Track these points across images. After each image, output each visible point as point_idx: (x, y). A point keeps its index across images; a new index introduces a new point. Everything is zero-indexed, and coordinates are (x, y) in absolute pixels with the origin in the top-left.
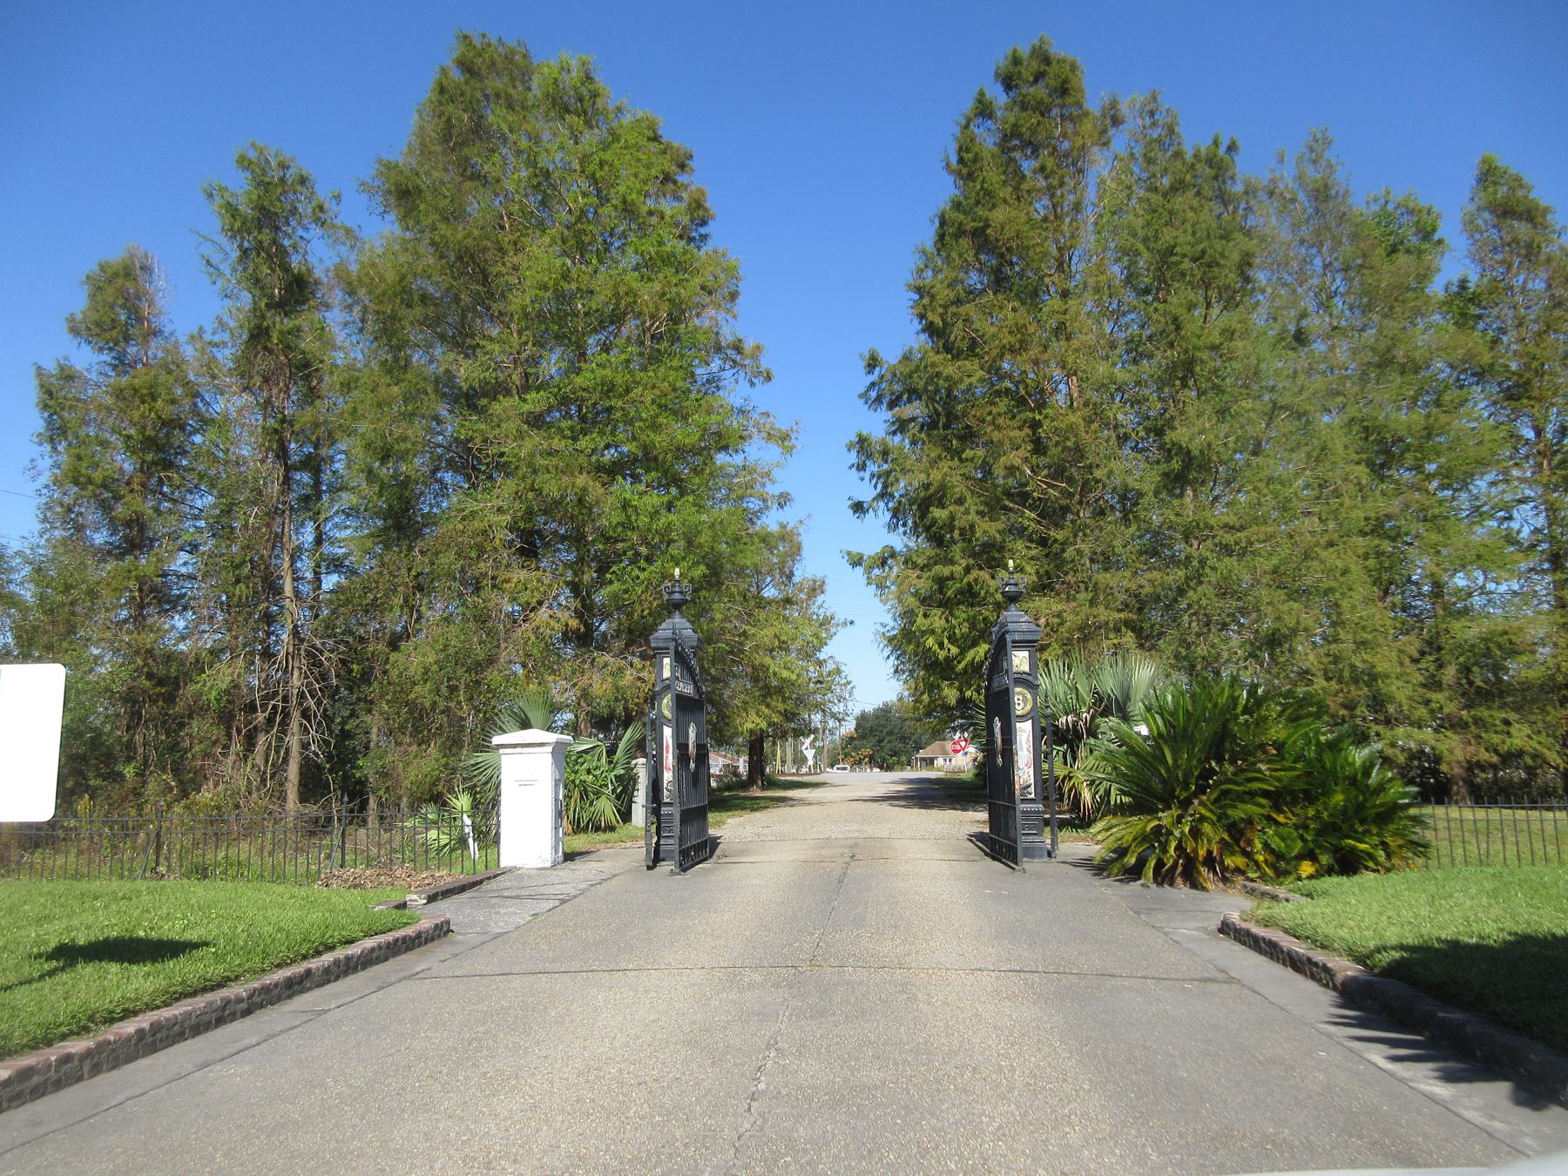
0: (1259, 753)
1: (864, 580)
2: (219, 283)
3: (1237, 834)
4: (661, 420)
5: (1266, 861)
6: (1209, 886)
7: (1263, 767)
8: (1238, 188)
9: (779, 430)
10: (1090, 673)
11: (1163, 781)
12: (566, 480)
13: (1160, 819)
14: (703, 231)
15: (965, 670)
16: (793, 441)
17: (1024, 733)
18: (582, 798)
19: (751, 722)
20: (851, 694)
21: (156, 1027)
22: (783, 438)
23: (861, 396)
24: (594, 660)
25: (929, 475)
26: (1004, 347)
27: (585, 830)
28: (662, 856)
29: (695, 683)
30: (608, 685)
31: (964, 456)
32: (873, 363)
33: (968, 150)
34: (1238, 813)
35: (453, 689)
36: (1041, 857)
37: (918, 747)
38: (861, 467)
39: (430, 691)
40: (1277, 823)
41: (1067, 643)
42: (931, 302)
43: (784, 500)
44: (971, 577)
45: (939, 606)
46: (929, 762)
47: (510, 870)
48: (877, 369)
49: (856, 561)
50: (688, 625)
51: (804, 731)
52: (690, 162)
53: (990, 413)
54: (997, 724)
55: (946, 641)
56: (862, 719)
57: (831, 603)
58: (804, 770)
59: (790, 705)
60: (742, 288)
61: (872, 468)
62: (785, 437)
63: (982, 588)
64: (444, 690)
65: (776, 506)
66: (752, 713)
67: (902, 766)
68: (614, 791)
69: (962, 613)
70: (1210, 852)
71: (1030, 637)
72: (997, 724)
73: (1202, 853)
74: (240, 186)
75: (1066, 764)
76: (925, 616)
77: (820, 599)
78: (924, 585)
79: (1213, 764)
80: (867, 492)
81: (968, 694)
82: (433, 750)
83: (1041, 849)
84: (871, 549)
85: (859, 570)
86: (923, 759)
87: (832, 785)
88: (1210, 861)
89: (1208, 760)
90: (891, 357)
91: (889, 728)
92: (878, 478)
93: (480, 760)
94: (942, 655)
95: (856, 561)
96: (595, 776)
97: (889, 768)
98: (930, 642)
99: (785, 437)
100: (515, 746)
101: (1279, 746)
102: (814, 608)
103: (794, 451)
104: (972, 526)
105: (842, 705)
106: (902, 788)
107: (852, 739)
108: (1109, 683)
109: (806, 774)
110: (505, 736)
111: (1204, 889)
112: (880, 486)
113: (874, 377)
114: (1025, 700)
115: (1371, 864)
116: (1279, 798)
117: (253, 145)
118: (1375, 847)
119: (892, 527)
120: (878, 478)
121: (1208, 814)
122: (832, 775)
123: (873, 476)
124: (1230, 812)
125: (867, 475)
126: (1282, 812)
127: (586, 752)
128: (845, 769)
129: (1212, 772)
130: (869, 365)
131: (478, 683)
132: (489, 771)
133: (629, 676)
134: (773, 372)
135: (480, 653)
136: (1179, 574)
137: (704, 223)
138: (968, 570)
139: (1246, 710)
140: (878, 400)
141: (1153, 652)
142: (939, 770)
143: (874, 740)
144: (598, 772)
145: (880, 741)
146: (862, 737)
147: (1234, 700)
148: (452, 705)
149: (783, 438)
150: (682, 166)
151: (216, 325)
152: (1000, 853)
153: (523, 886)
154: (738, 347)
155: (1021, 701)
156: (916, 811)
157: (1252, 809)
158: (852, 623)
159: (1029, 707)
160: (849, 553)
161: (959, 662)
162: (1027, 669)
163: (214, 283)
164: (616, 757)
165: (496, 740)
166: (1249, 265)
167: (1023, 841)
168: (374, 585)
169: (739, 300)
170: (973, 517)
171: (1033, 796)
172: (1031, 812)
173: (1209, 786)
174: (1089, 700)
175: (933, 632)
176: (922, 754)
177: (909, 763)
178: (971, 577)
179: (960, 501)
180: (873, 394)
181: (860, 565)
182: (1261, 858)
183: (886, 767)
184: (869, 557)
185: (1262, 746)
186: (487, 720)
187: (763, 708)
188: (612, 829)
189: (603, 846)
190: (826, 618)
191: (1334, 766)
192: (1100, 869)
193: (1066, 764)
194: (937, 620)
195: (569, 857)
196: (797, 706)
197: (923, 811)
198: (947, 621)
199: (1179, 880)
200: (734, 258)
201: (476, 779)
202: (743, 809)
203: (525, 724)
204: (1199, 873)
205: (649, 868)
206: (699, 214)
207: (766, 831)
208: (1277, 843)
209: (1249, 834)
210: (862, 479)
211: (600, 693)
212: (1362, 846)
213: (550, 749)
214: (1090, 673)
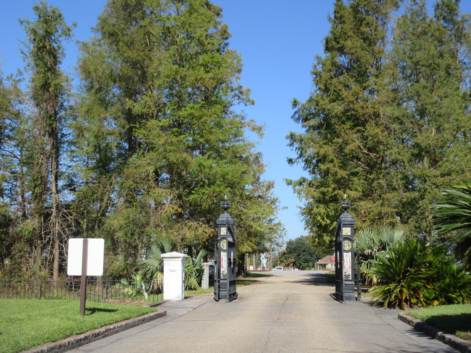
0: (423, 266)
1: (292, 191)
2: (27, 61)
3: (416, 291)
4: (214, 130)
5: (424, 301)
6: (405, 308)
7: (423, 270)
8: (459, 19)
9: (258, 126)
10: (379, 233)
11: (392, 274)
12: (178, 155)
13: (390, 286)
14: (226, 41)
15: (333, 230)
16: (263, 130)
17: (347, 258)
20: (285, 234)
21: (127, 324)
22: (258, 130)
23: (292, 117)
24: (186, 224)
26: (350, 102)
28: (220, 297)
31: (333, 141)
32: (295, 103)
33: (338, 13)
34: (414, 285)
35: (132, 234)
36: (353, 300)
37: (318, 259)
40: (427, 288)
41: (373, 221)
42: (320, 79)
44: (336, 192)
45: (323, 203)
46: (324, 266)
48: (297, 106)
49: (289, 183)
50: (230, 216)
51: (264, 250)
52: (221, 13)
53: (343, 128)
54: (338, 254)
55: (325, 218)
56: (290, 243)
57: (274, 193)
58: (259, 269)
60: (243, 68)
62: (260, 129)
63: (340, 197)
64: (129, 235)
66: (246, 244)
67: (310, 267)
68: (195, 275)
69: (332, 206)
70: (406, 297)
71: (351, 223)
72: (338, 254)
73: (404, 298)
74: (33, 17)
75: (368, 268)
76: (317, 207)
77: (272, 190)
78: (317, 194)
79: (409, 268)
80: (294, 155)
83: (353, 297)
84: (296, 178)
85: (291, 186)
87: (275, 276)
88: (406, 301)
89: (407, 267)
90: (303, 100)
92: (299, 149)
94: (323, 223)
95: (289, 183)
97: (303, 269)
98: (319, 218)
99: (260, 129)
101: (430, 263)
102: (269, 195)
103: (264, 135)
104: (336, 173)
105: (281, 239)
106: (308, 278)
107: (284, 253)
108: (385, 238)
109: (260, 271)
111: (404, 309)
112: (299, 152)
113: (296, 109)
114: (349, 245)
115: (456, 302)
116: (429, 280)
117: (41, 2)
118: (458, 296)
119: (305, 169)
120: (299, 149)
121: (404, 285)
122: (275, 271)
123: (296, 148)
124: (412, 284)
125: (294, 148)
126: (430, 285)
128: (280, 269)
129: (409, 271)
130: (294, 105)
132: (149, 266)
133: (200, 230)
134: (255, 101)
136: (416, 194)
137: (227, 38)
138: (334, 189)
139: (421, 251)
140: (299, 119)
141: (406, 225)
142: (328, 270)
143: (296, 254)
144: (189, 268)
145: (299, 255)
146: (290, 253)
147: (416, 247)
149: (258, 130)
150: (218, 15)
151: (18, 72)
152: (338, 298)
153: (175, 305)
155: (346, 245)
156: (312, 286)
157: (418, 283)
158: (287, 208)
159: (350, 248)
160: (286, 180)
161: (330, 226)
162: (350, 234)
163: (24, 61)
166: (450, 68)
167: (345, 295)
168: (96, 191)
169: (242, 73)
170: (337, 169)
171: (351, 279)
172: (349, 284)
173: (407, 276)
174: (378, 243)
175: (320, 214)
176: (320, 262)
177: (313, 266)
178: (336, 192)
179: (332, 161)
180: (297, 116)
181: (291, 184)
182: (422, 300)
183: (301, 268)
184: (295, 181)
185: (424, 263)
188: (195, 289)
189: (194, 295)
190: (274, 199)
191: (447, 270)
192: (371, 304)
193: (368, 268)
194: (322, 209)
195: (186, 298)
196: (261, 240)
197: (315, 286)
198: (326, 209)
199: (397, 307)
200: (239, 53)
202: (241, 284)
204: (402, 304)
206: (225, 34)
207: (253, 291)
208: (427, 295)
209: (419, 292)
211: (189, 237)
212: (453, 296)
213: (181, 259)
214: (379, 233)
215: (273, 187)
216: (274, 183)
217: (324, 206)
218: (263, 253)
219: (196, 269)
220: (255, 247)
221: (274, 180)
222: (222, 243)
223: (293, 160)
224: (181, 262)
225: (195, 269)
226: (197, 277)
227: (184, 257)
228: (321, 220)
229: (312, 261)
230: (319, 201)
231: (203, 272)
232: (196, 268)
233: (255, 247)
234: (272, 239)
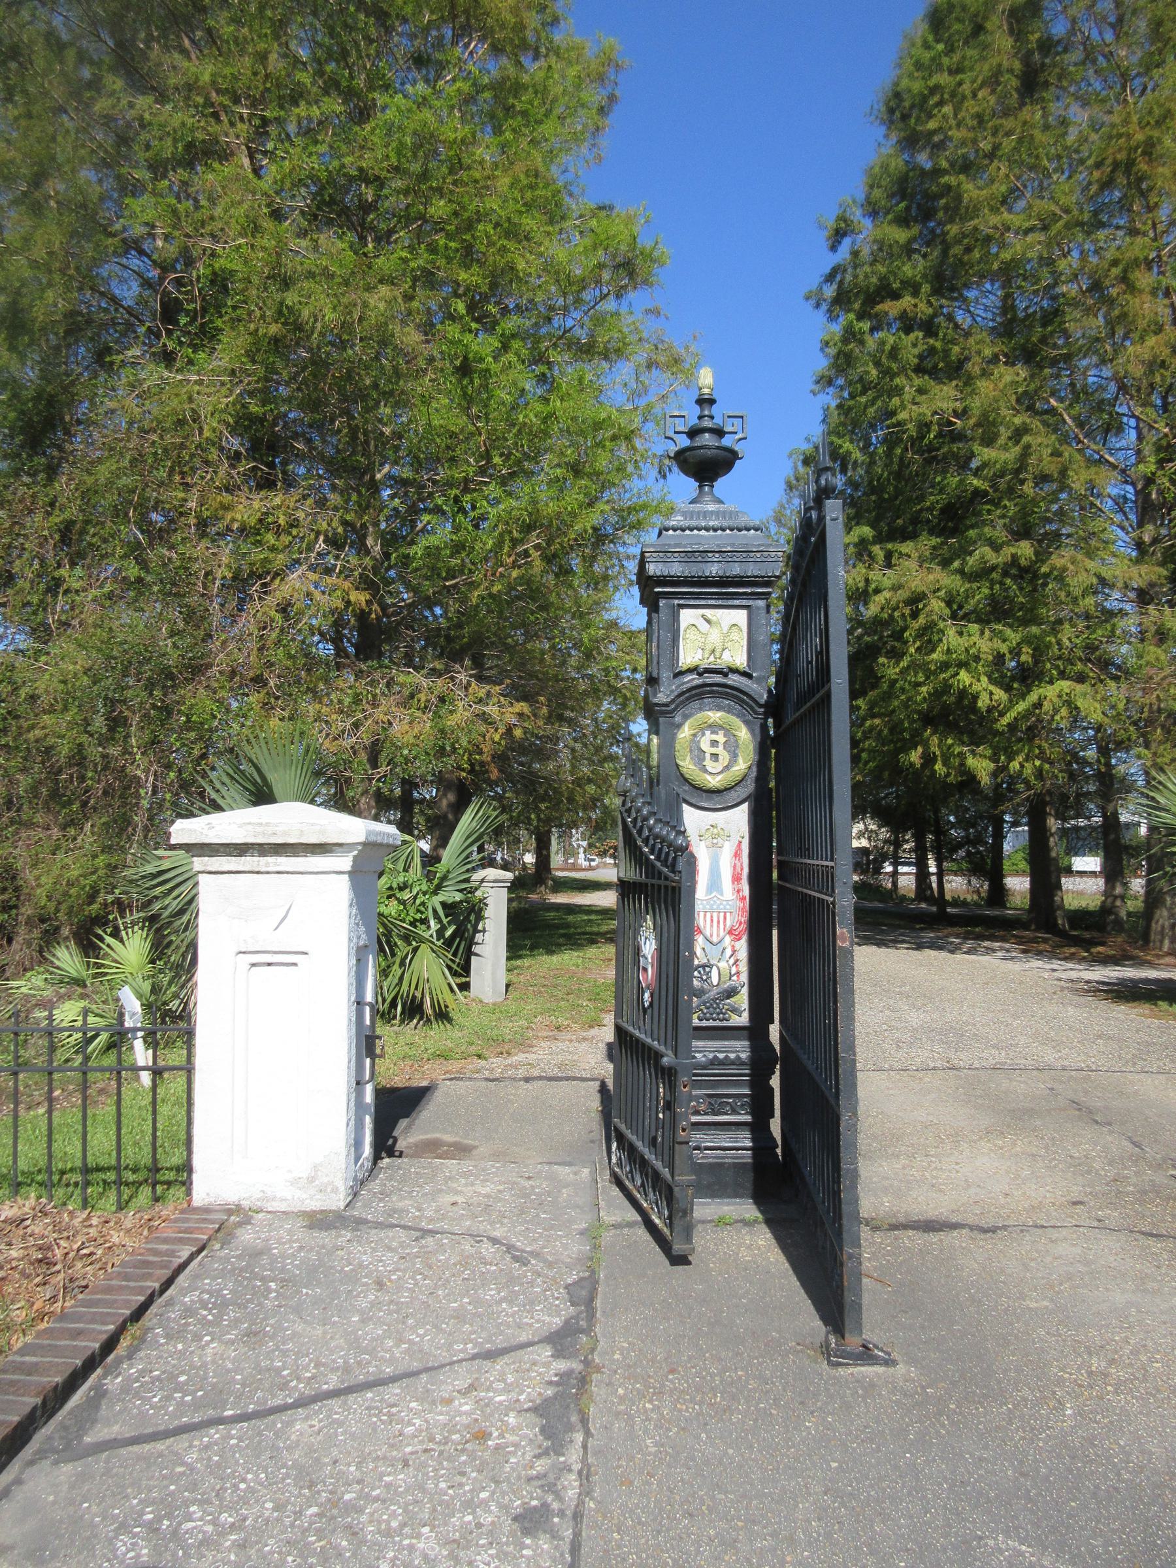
15: (1012, 727)
30: (426, 725)
35: (116, 723)
39: (71, 725)
64: (99, 723)
68: (440, 933)
82: (88, 837)
93: (166, 865)
96: (403, 902)
100: (241, 850)
110: (215, 818)
131: (167, 711)
144: (406, 895)
148: (114, 751)
161: (1002, 714)
165: (183, 830)
183: (402, 831)
186: (185, 785)
201: (157, 906)
203: (262, 795)
213: (345, 862)
219: (444, 905)
222: (685, 733)
224: (343, 885)
225: (436, 901)
226: (449, 943)
227: (370, 847)
231: (480, 917)
232: (442, 897)
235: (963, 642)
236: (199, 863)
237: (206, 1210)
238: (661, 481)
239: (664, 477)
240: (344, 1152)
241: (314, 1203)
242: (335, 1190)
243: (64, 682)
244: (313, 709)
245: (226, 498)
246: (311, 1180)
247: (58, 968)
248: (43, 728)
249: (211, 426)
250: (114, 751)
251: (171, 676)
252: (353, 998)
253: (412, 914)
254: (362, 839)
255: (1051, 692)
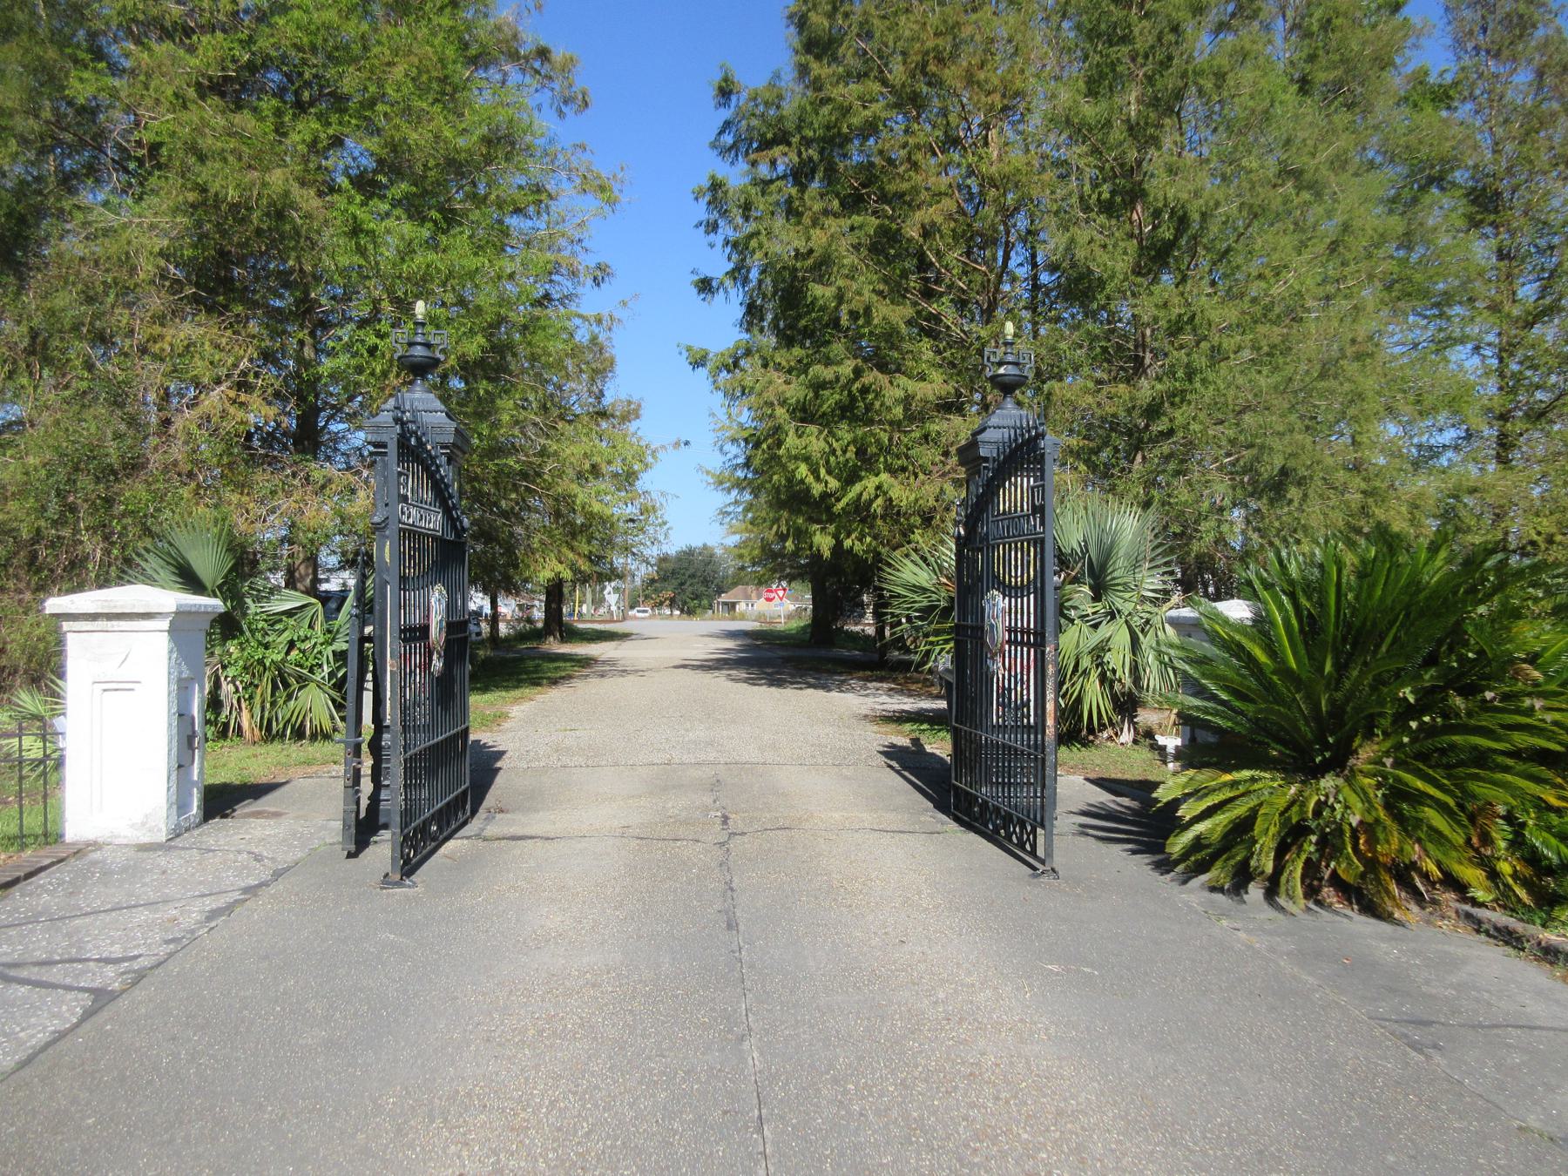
5: (1515, 876)
18: (275, 688)
19: (547, 569)
25: (808, 239)
27: (281, 736)
29: (447, 511)
32: (725, 92)
37: (720, 591)
38: (712, 227)
43: (601, 275)
47: (80, 851)
48: (734, 98)
50: (438, 405)
51: (614, 575)
59: (595, 547)
61: (726, 231)
65: (589, 282)
80: (718, 264)
81: (848, 543)
85: (702, 372)
86: (725, 604)
90: (752, 80)
91: (691, 571)
94: (817, 489)
96: (303, 652)
98: (803, 470)
100: (94, 617)
104: (868, 310)
105: (655, 548)
107: (653, 581)
112: (735, 257)
113: (726, 114)
125: (718, 239)
127: (290, 613)
131: (109, 502)
135: (113, 453)
138: (858, 372)
143: (675, 583)
144: (307, 645)
145: (682, 584)
146: (664, 579)
154: (543, 54)
158: (687, 443)
160: (689, 349)
161: (838, 500)
164: (337, 623)
176: (724, 598)
180: (728, 139)
187: (565, 550)
189: (300, 771)
197: (773, 689)
205: (350, 855)
210: (712, 246)
213: (165, 624)
215: (638, 417)
216: (639, 405)
217: (821, 432)
218: (610, 580)
220: (585, 566)
221: (642, 399)
223: (714, 284)
224: (164, 639)
225: (330, 650)
228: (810, 479)
229: (708, 596)
230: (804, 414)
233: (585, 566)
234: (632, 546)
235: (800, 443)
236: (66, 626)
237: (73, 844)
238: (596, 288)
239: (598, 285)
240: (165, 806)
241: (146, 839)
242: (160, 830)
243: (27, 474)
244: (235, 498)
245: (157, 329)
246: (143, 824)
247: (19, 706)
248: (8, 513)
249: (147, 268)
250: (66, 533)
251: (114, 472)
252: (174, 710)
253: (311, 661)
254: (174, 610)
255: (869, 484)
